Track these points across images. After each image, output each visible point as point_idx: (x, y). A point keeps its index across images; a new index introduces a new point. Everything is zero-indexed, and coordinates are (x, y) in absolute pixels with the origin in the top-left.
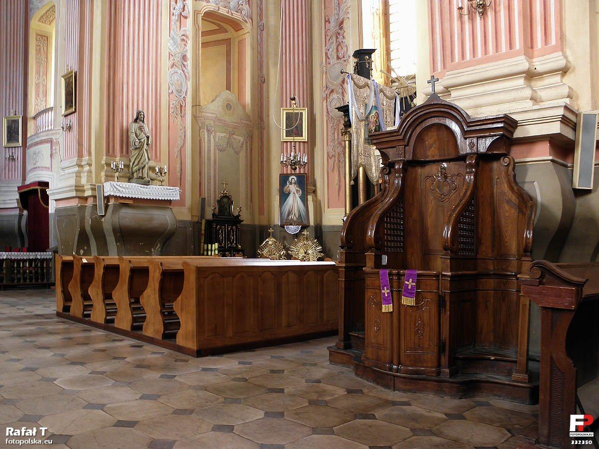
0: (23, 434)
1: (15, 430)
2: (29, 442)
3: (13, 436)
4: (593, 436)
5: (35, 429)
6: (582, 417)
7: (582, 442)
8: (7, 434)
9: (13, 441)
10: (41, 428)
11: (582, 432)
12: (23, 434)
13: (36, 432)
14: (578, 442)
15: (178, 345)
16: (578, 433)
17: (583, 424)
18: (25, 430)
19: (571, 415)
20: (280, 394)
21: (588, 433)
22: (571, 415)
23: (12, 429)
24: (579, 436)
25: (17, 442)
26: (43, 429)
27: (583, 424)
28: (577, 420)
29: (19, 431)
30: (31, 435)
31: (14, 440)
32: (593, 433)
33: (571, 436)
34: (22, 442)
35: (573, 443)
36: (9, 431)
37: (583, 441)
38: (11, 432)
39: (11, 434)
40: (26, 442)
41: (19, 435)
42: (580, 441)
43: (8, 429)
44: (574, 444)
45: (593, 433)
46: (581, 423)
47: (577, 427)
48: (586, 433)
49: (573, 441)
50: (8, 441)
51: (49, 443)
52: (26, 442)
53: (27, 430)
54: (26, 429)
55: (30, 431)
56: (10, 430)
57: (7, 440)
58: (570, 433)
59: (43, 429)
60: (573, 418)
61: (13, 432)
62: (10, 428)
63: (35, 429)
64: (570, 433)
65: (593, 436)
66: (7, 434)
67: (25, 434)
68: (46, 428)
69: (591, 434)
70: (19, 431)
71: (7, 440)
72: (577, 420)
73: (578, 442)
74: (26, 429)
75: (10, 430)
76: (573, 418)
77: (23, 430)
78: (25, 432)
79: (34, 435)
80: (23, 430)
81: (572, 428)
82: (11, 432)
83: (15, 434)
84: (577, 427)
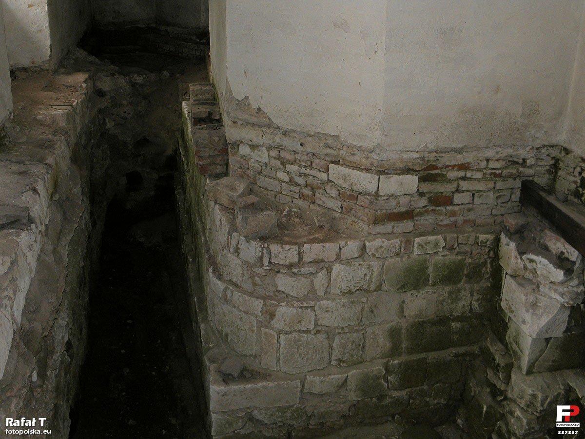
0: (22, 425)
3: (13, 426)
4: (579, 426)
5: (34, 419)
6: (568, 407)
7: (568, 432)
8: (7, 425)
9: (13, 432)
10: (40, 419)
11: (569, 422)
12: (22, 425)
14: (565, 432)
16: (564, 423)
18: (24, 421)
19: (558, 406)
21: (575, 424)
22: (558, 406)
24: (565, 426)
25: (17, 432)
26: (42, 420)
28: (564, 411)
31: (13, 430)
32: (579, 423)
34: (21, 432)
35: (559, 433)
36: (9, 421)
37: (570, 431)
38: (10, 423)
39: (11, 425)
41: (19, 425)
42: (566, 431)
43: (7, 419)
45: (579, 423)
46: (568, 414)
48: (573, 423)
49: (560, 431)
50: (8, 432)
53: (27, 421)
55: (30, 421)
56: (10, 420)
57: (6, 430)
58: (557, 423)
60: (560, 408)
61: (13, 423)
62: (10, 419)
63: (34, 419)
64: (557, 423)
65: (579, 426)
66: (7, 425)
68: (45, 419)
69: (577, 425)
70: (18, 422)
71: (6, 430)
72: (564, 411)
73: (565, 432)
74: (26, 420)
75: (10, 420)
76: (560, 408)
78: (25, 422)
79: (34, 425)
81: (559, 418)
82: (10, 423)
83: (26, 425)
84: (564, 418)
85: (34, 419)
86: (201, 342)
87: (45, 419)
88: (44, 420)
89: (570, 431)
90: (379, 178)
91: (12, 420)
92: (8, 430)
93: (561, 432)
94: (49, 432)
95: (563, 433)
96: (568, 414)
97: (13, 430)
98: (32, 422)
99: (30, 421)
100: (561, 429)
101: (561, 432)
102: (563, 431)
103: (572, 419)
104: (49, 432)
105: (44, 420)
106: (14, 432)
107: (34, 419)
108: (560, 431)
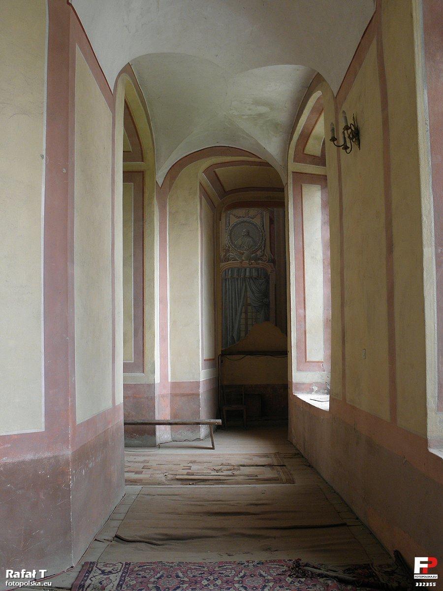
0: (23, 577)
1: (15, 573)
2: (28, 584)
3: (13, 578)
4: (437, 578)
5: (34, 571)
6: (426, 559)
7: (426, 584)
8: (7, 577)
9: (13, 583)
10: (40, 571)
11: (426, 574)
12: (23, 577)
13: (36, 575)
14: (423, 584)
15: (46, 427)
16: (422, 575)
17: (427, 567)
18: (25, 573)
19: (415, 558)
20: (294, 171)
21: (432, 575)
22: (415, 558)
23: (12, 572)
24: (423, 578)
25: (17, 584)
26: (43, 571)
27: (427, 567)
28: (422, 562)
29: (18, 573)
30: (30, 577)
31: (14, 582)
32: (437, 575)
34: (21, 584)
35: (417, 585)
36: (9, 573)
37: (428, 583)
38: (11, 574)
39: (11, 577)
40: (26, 584)
41: (19, 577)
42: (424, 583)
43: (8, 571)
44: (429, 586)
45: (437, 575)
46: (426, 566)
47: (421, 569)
48: (431, 575)
49: (417, 583)
50: (8, 584)
51: (49, 585)
52: (26, 584)
53: (27, 573)
54: (26, 571)
55: (30, 573)
56: (10, 572)
57: (6, 583)
58: (415, 575)
59: (43, 571)
60: (418, 560)
61: (13, 575)
62: (10, 571)
63: (34, 571)
64: (415, 575)
65: (437, 578)
66: (7, 577)
67: (24, 576)
68: (46, 571)
69: (435, 577)
70: (18, 573)
71: (6, 583)
72: (422, 562)
73: (423, 584)
74: (26, 571)
75: (10, 572)
76: (418, 560)
77: (23, 572)
78: (25, 574)
79: (34, 577)
80: (23, 572)
81: (417, 570)
82: (11, 574)
83: (27, 576)
84: (421, 569)
85: (34, 571)
86: (251, 165)
87: (46, 571)
88: (45, 572)
89: (428, 583)
90: (127, 472)
91: (12, 572)
92: (8, 582)
93: (419, 584)
94: (49, 584)
95: (421, 585)
96: (426, 566)
97: (14, 582)
98: (32, 574)
99: (30, 573)
100: (419, 581)
101: (419, 584)
102: (421, 583)
103: (429, 571)
104: (49, 584)
105: (45, 572)
106: (15, 584)
107: (34, 571)
108: (417, 583)
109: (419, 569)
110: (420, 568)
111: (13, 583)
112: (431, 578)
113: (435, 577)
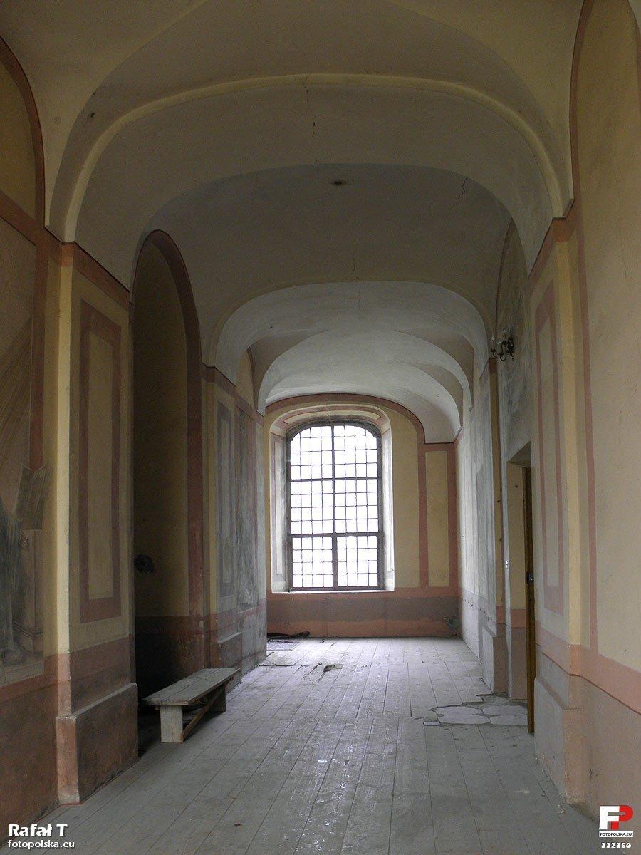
0: (33, 834)
1: (22, 828)
5: (49, 826)
6: (616, 809)
8: (10, 834)
10: (58, 826)
12: (33, 834)
16: (611, 832)
18: (36, 828)
21: (626, 833)
26: (62, 826)
28: (610, 814)
31: (20, 842)
32: (632, 832)
33: (602, 836)
35: (604, 847)
36: (13, 829)
38: (15, 831)
39: (16, 834)
41: (27, 835)
43: (11, 826)
45: (632, 832)
46: (616, 818)
49: (604, 844)
50: (11, 844)
53: (39, 829)
54: (37, 827)
55: (43, 829)
56: (14, 828)
59: (62, 826)
60: (604, 810)
61: (19, 831)
63: (49, 826)
65: (632, 836)
66: (10, 834)
67: (35, 833)
68: (66, 825)
71: (9, 843)
72: (610, 814)
74: (37, 827)
75: (14, 828)
76: (604, 810)
78: (36, 831)
79: (49, 834)
81: (603, 825)
83: (21, 834)
87: (66, 825)
91: (17, 827)
94: (71, 845)
97: (20, 842)
104: (71, 845)
109: (606, 824)
110: (608, 822)
111: (18, 844)
112: (624, 836)
113: (630, 834)
